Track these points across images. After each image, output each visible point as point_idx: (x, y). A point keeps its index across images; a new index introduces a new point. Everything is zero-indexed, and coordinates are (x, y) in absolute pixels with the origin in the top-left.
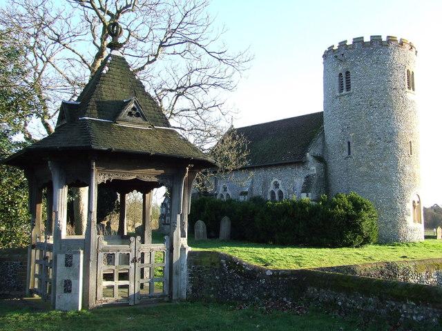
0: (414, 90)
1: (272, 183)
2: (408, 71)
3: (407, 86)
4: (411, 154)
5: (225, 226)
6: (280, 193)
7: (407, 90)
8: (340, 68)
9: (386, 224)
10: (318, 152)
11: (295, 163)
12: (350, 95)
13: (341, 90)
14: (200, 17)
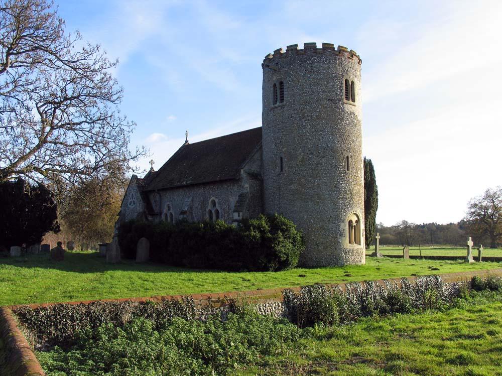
0: (353, 100)
1: (211, 200)
2: (346, 81)
3: (344, 96)
4: (348, 170)
5: (143, 248)
6: (217, 212)
7: (345, 101)
8: (275, 78)
9: (317, 245)
10: (254, 168)
11: (187, 186)
12: (283, 107)
13: (275, 102)
14: (33, 13)
